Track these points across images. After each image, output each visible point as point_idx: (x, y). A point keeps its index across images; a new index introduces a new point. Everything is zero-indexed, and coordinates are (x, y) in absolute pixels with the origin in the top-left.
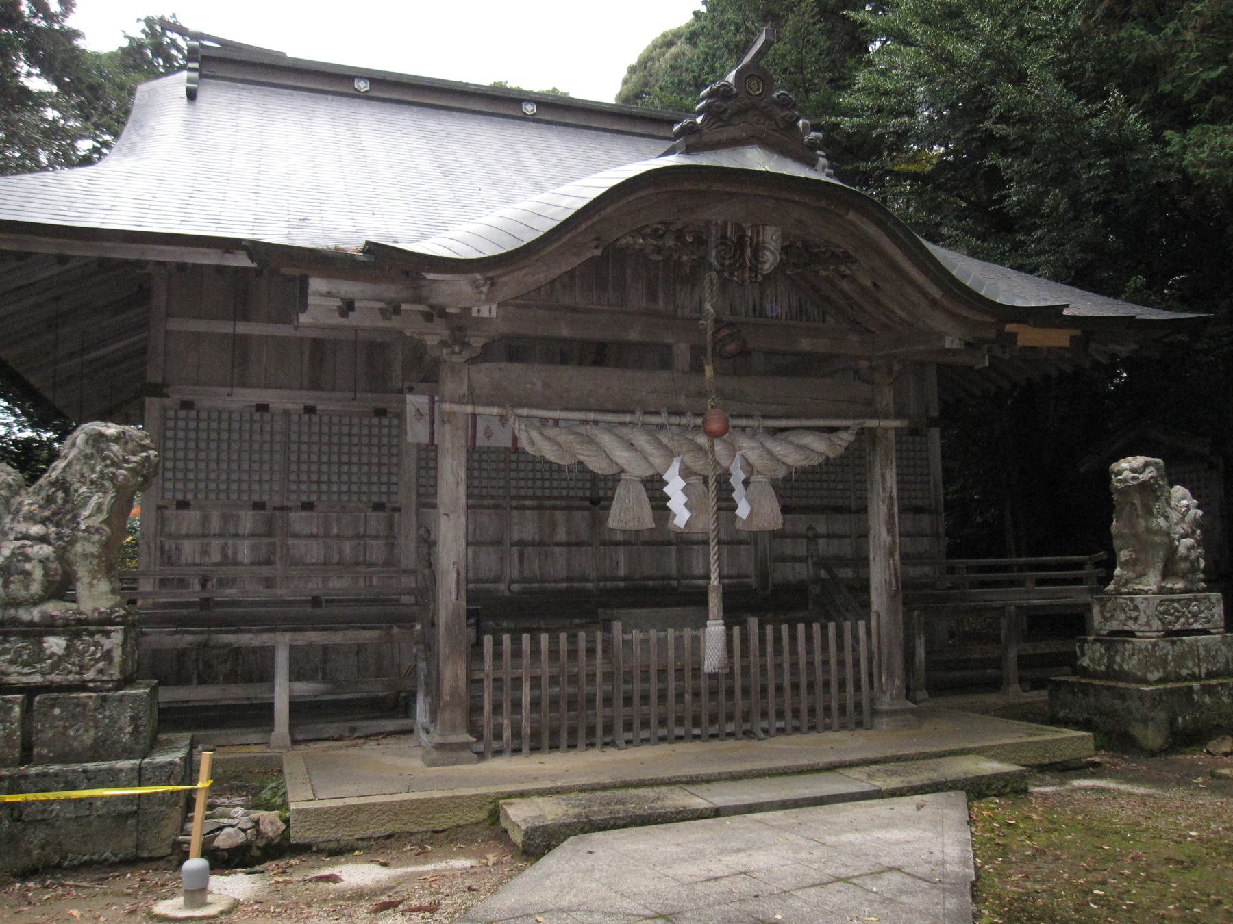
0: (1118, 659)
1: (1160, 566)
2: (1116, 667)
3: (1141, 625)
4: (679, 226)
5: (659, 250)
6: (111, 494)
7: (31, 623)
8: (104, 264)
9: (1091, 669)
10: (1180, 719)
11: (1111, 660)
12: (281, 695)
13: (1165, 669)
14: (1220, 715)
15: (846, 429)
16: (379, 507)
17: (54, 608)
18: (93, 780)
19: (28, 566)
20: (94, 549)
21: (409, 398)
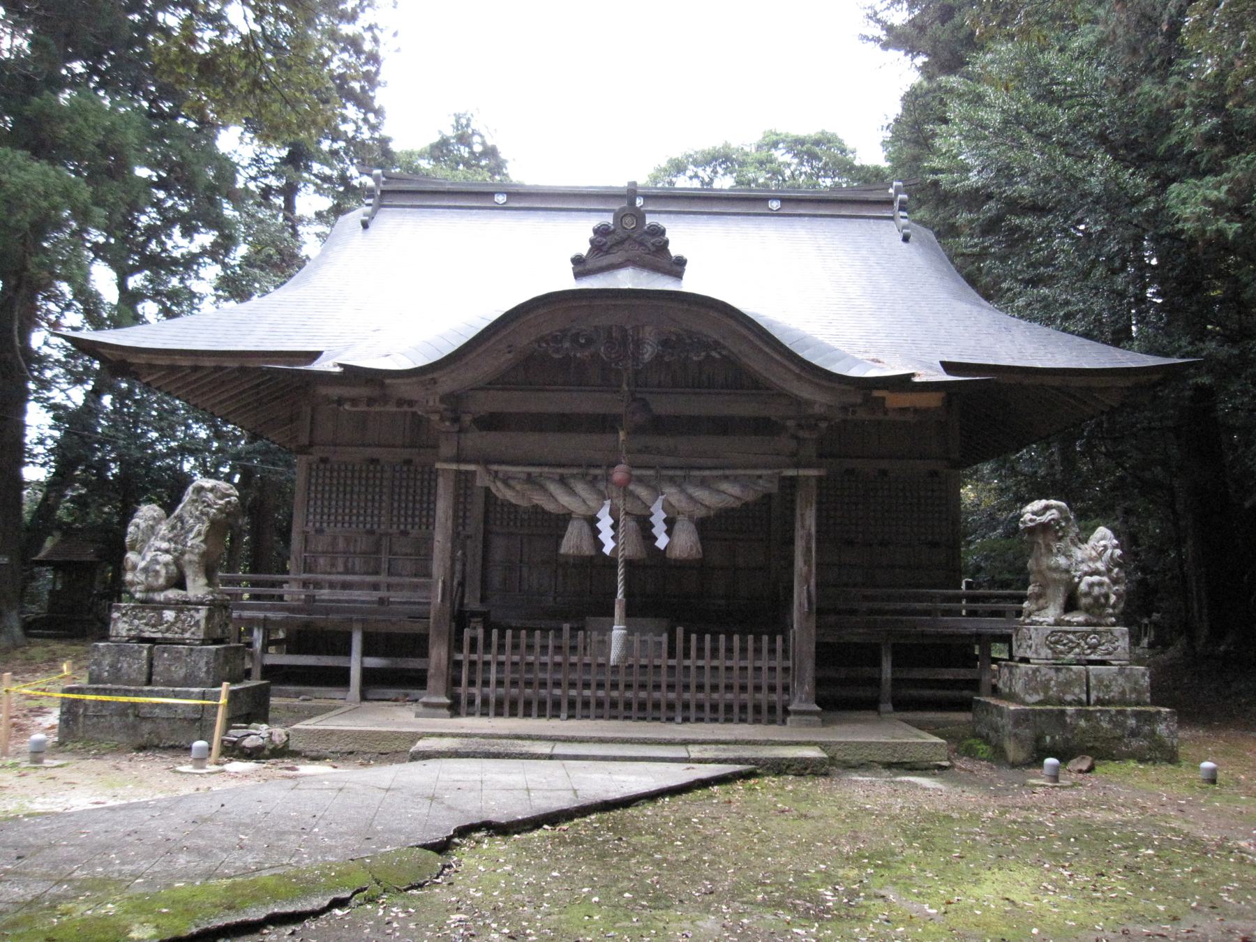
1: (1061, 600)
4: (574, 331)
5: (557, 351)
6: (207, 524)
7: (160, 602)
8: (243, 370)
10: (1048, 738)
12: (355, 664)
13: (1046, 693)
14: (1096, 739)
17: (172, 594)
18: (176, 695)
19: (158, 567)
20: (196, 558)
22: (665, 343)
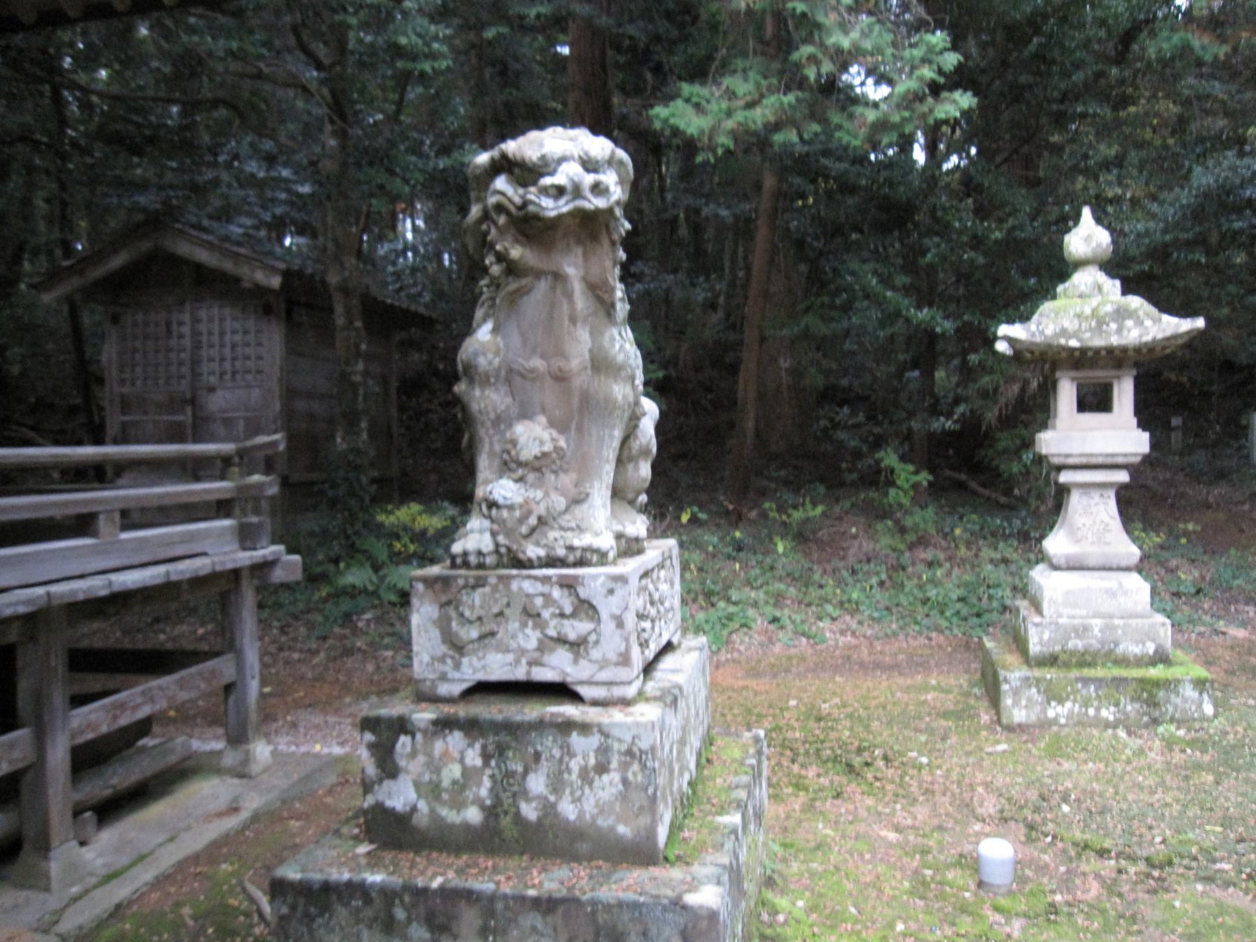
0: (537, 783)
2: (530, 812)
3: (603, 664)
9: (423, 816)
11: (509, 787)
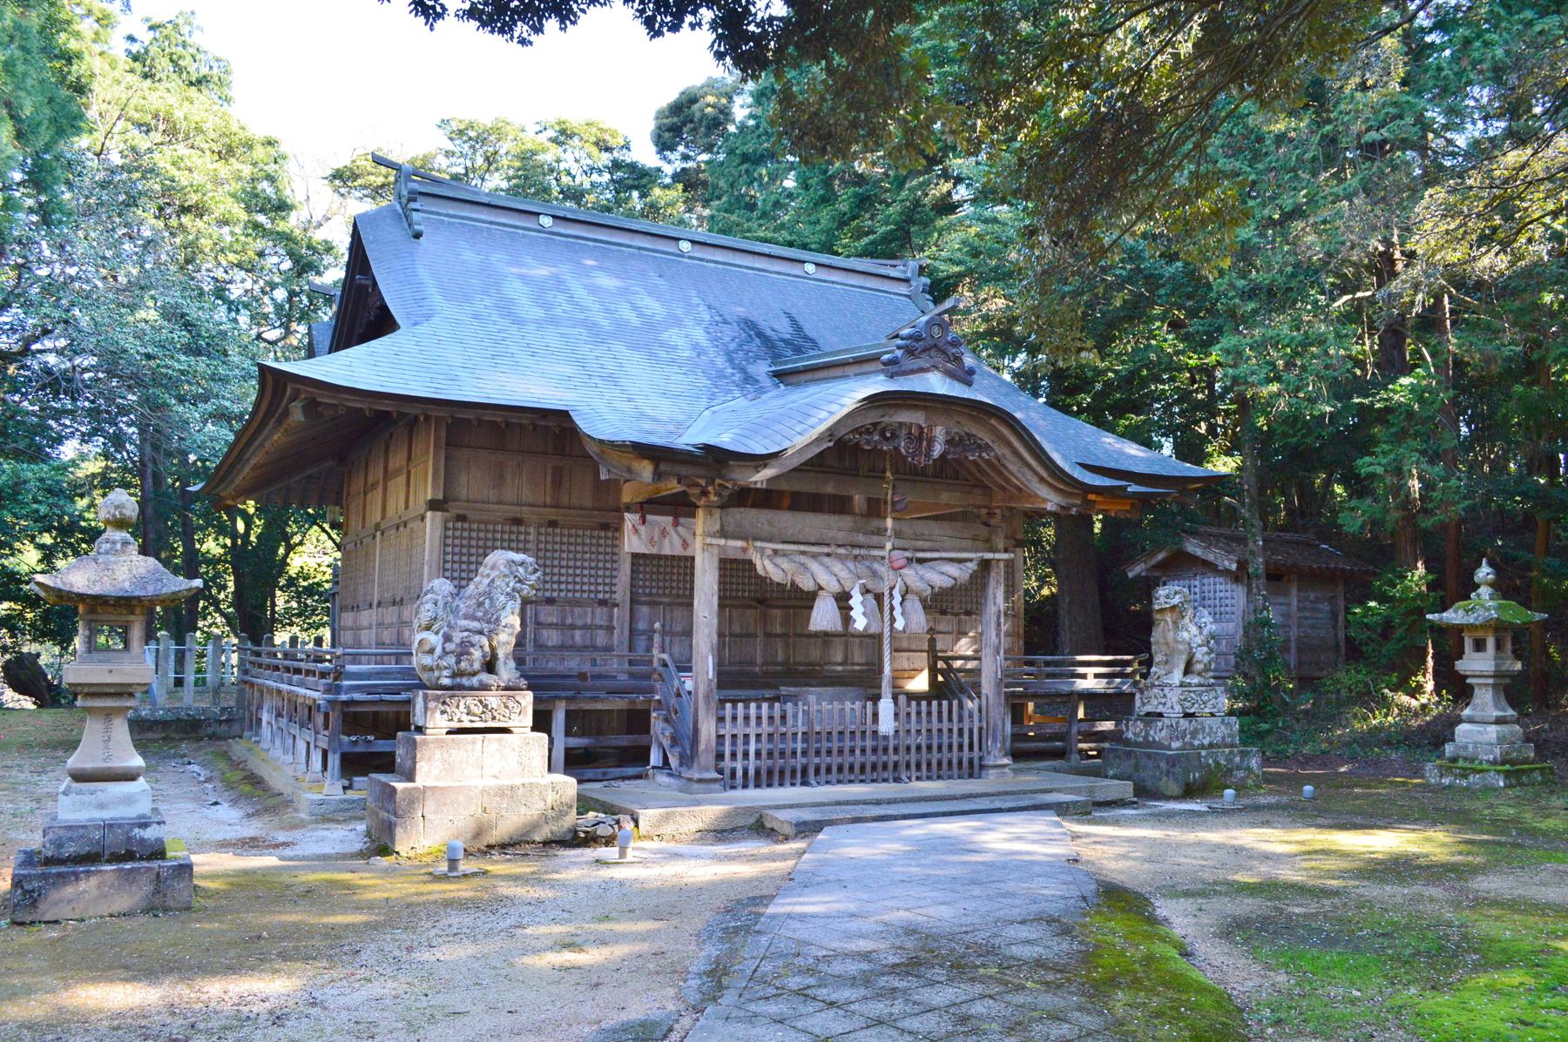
1: (1182, 667)
5: (868, 442)
11: (1147, 734)
15: (971, 560)
16: (603, 603)
21: (627, 515)
22: (949, 442)
